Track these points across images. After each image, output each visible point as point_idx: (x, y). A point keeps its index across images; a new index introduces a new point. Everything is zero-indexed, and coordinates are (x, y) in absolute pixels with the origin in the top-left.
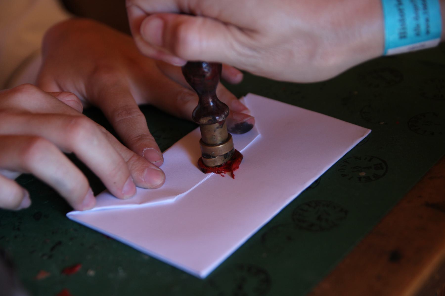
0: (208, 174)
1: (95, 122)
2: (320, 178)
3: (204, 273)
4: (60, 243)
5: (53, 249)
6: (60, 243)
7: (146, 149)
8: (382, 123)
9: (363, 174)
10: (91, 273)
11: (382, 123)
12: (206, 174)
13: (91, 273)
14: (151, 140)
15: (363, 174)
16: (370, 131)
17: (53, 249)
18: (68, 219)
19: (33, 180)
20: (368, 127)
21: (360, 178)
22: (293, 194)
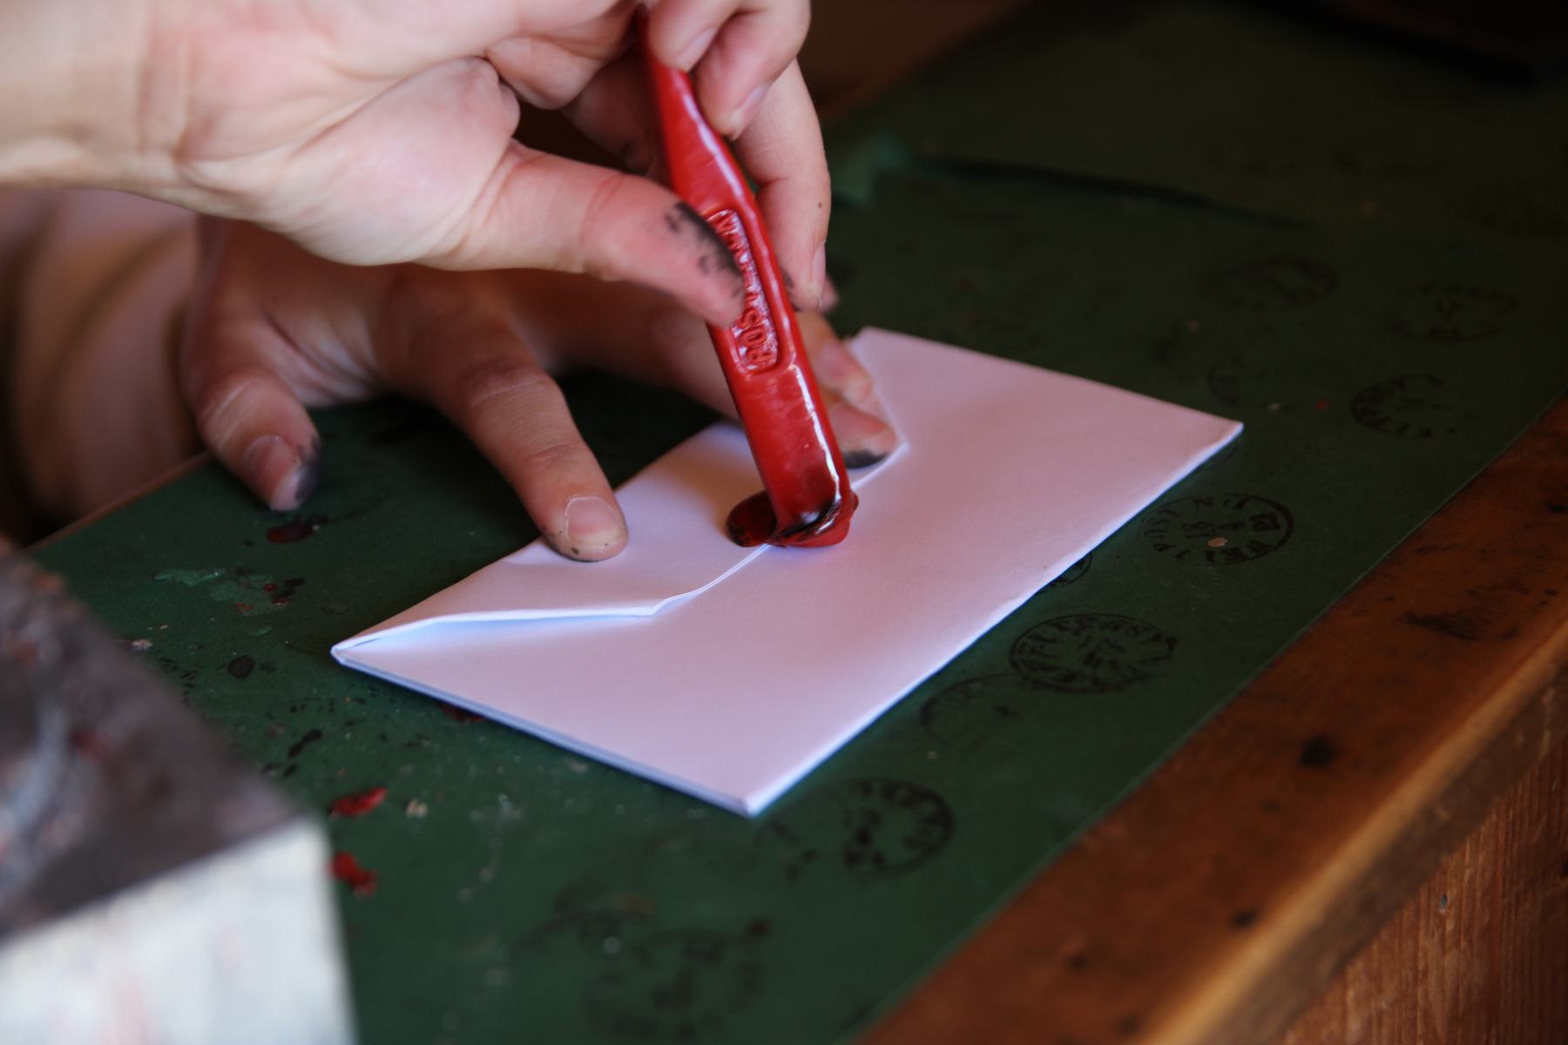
0: (754, 548)
1: (525, 548)
2: (1090, 555)
3: (757, 801)
4: (315, 735)
5: (295, 750)
6: (315, 735)
7: (575, 499)
8: (1275, 407)
9: (1220, 543)
10: (418, 810)
11: (1275, 407)
12: (745, 549)
13: (418, 810)
14: (585, 466)
15: (1220, 543)
16: (1237, 428)
17: (295, 750)
18: (334, 662)
19: (216, 574)
20: (1233, 416)
21: (1210, 555)
22: (1012, 598)
